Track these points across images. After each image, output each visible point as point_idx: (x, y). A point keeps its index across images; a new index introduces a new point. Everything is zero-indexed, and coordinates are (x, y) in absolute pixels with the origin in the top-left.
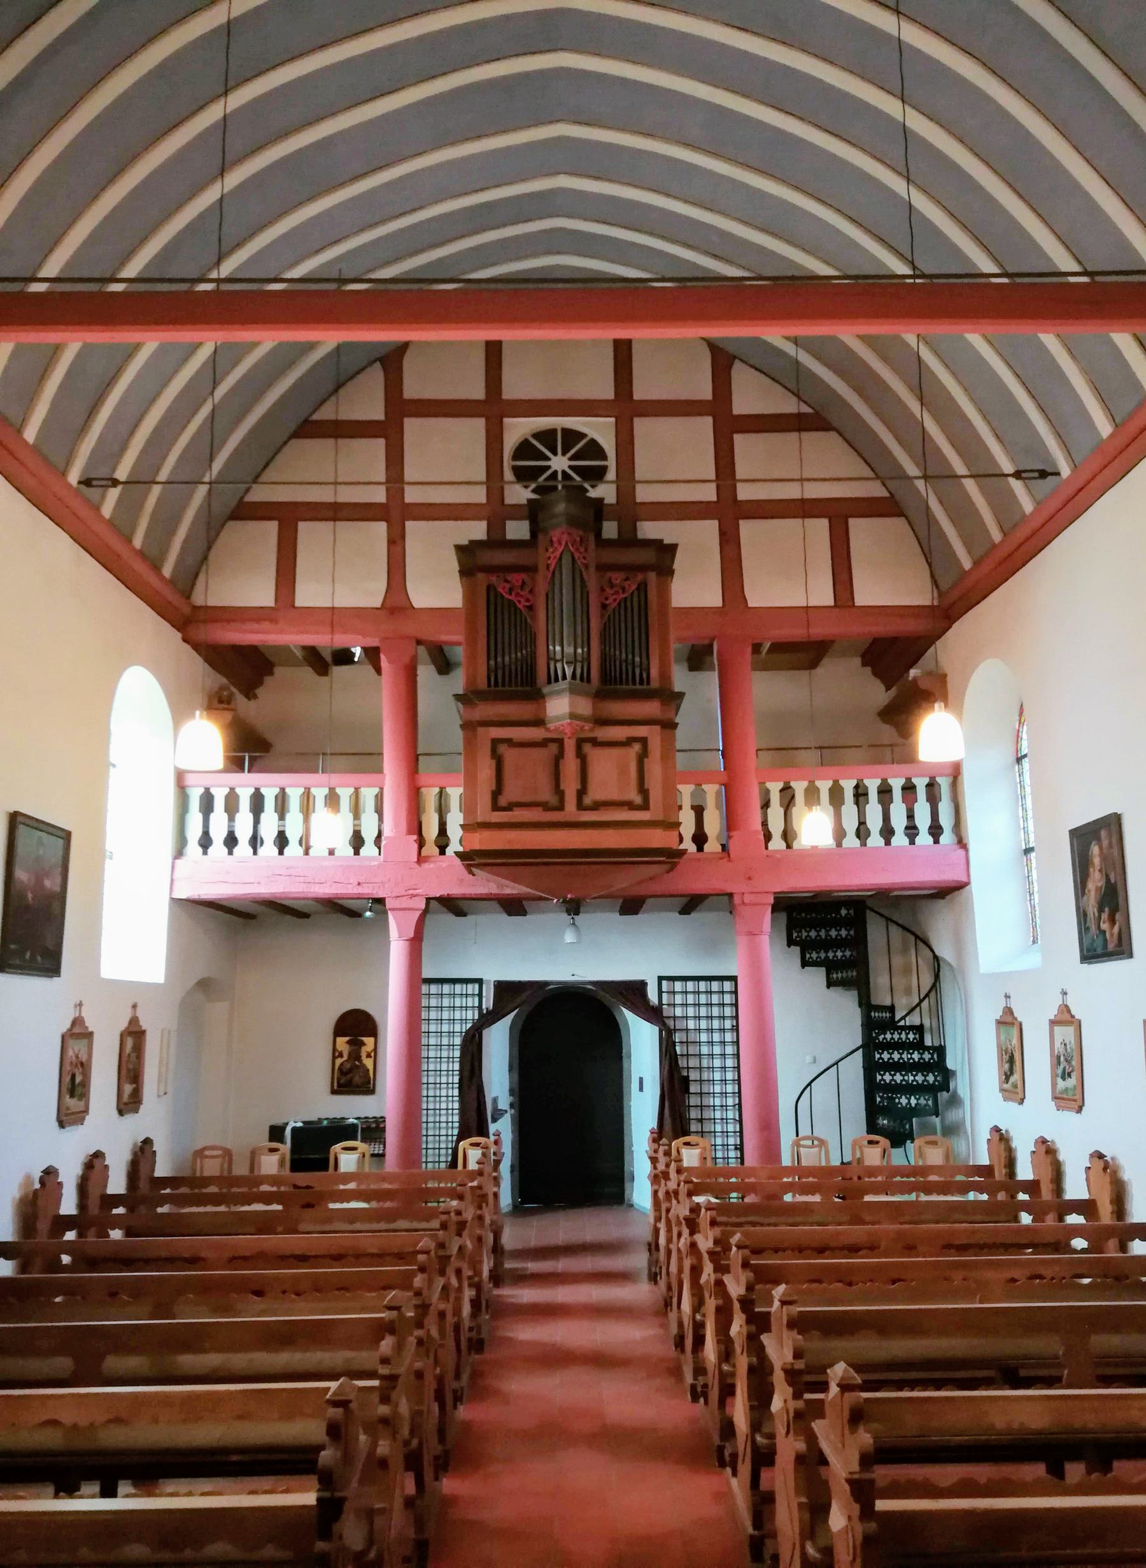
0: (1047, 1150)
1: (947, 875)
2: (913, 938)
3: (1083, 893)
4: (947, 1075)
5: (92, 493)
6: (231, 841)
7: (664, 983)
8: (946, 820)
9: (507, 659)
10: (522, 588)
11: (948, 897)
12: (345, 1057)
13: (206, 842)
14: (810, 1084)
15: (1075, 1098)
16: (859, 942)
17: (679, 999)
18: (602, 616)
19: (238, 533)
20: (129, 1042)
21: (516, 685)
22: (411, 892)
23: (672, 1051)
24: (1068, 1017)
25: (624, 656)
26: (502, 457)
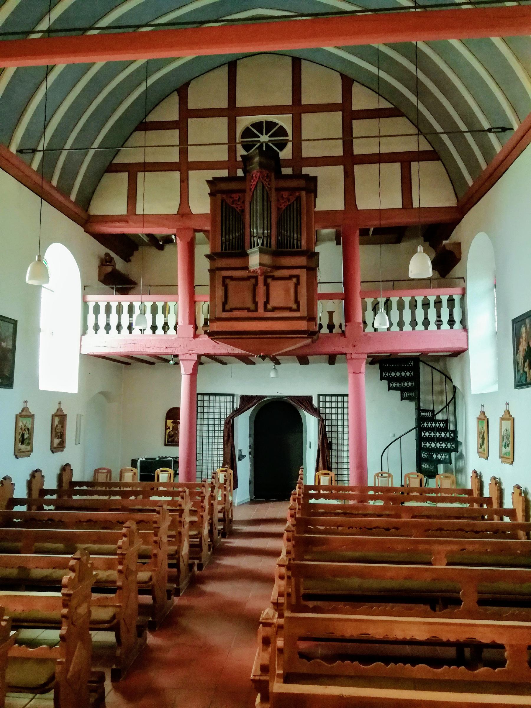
0: (497, 483)
1: (457, 345)
2: (444, 377)
3: (517, 353)
4: (458, 444)
5: (26, 157)
6: (108, 327)
7: (321, 397)
8: (457, 317)
9: (231, 236)
10: (239, 200)
11: (459, 356)
12: (171, 429)
13: (96, 328)
14: (387, 447)
15: (509, 457)
16: (416, 379)
17: (328, 405)
18: (278, 214)
19: (108, 178)
20: (57, 420)
21: (235, 250)
22: (190, 352)
23: (324, 430)
24: (508, 416)
25: (289, 234)
26: (236, 138)
